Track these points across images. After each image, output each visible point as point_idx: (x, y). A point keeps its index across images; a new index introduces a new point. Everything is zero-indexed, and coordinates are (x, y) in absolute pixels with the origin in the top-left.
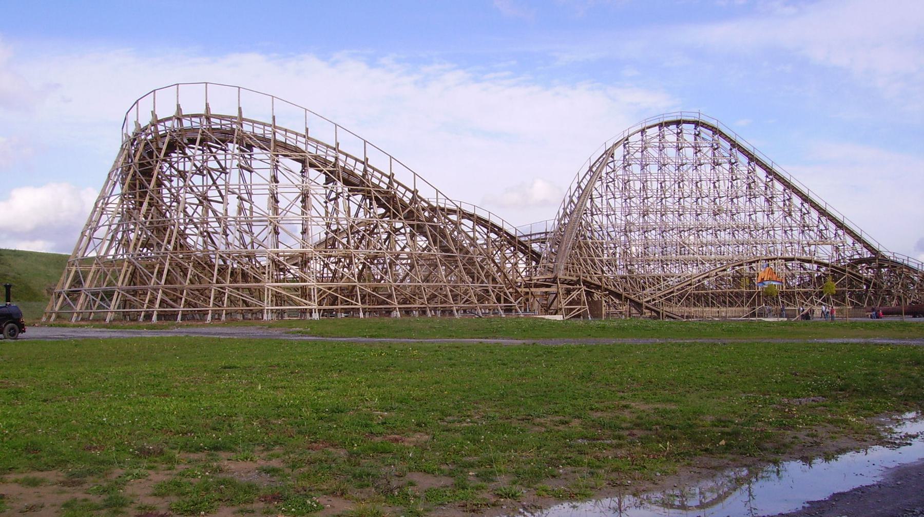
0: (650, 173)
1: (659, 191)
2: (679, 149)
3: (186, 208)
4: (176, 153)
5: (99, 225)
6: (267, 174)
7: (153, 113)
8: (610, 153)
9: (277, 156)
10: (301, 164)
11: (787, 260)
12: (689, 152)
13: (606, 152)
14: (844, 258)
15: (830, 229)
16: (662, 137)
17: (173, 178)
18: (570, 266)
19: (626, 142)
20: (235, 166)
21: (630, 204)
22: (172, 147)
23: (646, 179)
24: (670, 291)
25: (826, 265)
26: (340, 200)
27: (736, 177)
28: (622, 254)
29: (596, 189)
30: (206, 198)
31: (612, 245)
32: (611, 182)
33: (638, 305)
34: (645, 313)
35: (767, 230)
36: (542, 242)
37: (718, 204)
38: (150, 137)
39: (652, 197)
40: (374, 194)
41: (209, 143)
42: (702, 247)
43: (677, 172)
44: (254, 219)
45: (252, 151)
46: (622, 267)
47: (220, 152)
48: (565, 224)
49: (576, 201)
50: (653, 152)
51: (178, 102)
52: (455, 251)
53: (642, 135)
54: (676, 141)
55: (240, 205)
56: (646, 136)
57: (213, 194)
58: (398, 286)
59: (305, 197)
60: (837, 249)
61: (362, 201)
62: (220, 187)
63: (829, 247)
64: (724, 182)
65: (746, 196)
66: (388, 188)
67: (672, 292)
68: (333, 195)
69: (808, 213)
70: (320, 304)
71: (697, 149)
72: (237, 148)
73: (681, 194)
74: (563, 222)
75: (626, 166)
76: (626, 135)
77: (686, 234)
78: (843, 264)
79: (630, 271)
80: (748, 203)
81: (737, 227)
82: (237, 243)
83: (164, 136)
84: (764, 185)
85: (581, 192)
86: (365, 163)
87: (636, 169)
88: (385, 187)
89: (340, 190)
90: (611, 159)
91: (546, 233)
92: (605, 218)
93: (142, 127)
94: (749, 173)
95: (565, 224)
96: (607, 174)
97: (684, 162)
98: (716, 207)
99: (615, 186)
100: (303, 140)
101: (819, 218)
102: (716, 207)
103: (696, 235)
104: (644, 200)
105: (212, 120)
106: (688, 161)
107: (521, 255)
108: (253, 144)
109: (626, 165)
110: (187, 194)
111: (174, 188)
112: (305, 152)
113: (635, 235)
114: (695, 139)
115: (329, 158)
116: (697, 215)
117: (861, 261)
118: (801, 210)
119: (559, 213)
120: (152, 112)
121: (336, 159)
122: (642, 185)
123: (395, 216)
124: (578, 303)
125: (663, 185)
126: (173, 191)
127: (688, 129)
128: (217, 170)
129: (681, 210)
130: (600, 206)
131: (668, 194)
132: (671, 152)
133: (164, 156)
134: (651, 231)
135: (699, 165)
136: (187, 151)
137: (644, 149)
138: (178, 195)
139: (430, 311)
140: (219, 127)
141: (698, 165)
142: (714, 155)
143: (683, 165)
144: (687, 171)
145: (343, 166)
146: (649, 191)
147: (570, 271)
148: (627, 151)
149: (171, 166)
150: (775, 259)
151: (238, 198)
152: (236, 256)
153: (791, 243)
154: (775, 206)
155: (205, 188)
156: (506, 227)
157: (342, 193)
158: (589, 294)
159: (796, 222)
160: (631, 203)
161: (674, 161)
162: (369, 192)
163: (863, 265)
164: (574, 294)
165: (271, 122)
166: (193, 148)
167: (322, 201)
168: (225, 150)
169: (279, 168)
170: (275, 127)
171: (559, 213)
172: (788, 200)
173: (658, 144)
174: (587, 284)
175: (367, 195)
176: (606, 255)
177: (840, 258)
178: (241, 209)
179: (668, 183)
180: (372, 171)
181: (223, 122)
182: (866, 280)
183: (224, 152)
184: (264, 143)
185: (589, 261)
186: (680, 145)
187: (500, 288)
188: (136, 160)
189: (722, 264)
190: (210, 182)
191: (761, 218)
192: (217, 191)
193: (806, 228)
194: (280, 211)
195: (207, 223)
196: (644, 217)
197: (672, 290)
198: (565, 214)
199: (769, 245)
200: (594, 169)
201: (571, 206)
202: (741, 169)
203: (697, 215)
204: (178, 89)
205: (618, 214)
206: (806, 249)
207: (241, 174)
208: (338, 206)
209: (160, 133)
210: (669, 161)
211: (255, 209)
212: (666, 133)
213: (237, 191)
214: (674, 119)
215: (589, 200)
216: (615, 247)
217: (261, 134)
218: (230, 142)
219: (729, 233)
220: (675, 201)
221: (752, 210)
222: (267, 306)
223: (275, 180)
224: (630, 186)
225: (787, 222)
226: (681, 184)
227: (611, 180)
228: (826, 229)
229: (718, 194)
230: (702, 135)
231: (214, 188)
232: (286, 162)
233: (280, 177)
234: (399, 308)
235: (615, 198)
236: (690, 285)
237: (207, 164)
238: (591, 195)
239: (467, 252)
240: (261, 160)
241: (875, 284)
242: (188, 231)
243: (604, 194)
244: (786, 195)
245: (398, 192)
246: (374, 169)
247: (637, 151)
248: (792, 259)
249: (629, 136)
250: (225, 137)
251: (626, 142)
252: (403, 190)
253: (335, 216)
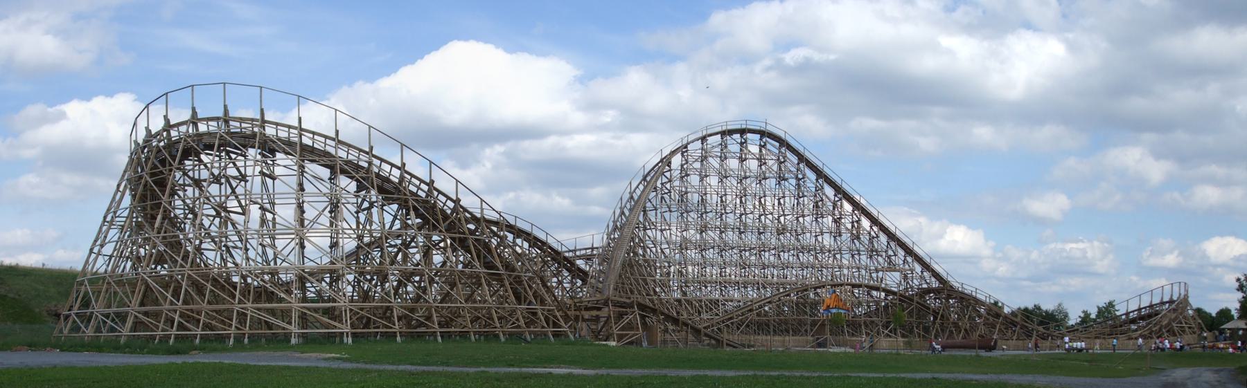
0: (709, 185)
1: (719, 205)
2: (742, 160)
3: (202, 220)
4: (191, 160)
5: (107, 241)
6: (293, 181)
7: (166, 117)
8: (666, 161)
9: (303, 161)
10: (329, 170)
11: (854, 286)
12: (753, 164)
13: (662, 161)
14: (912, 287)
15: (899, 255)
16: (724, 146)
17: (186, 188)
18: (620, 285)
19: (684, 150)
20: (257, 173)
21: (687, 219)
22: (187, 154)
23: (706, 191)
24: (729, 316)
25: (894, 293)
26: (374, 210)
27: (803, 193)
28: (677, 273)
29: (650, 201)
30: (225, 210)
31: (666, 264)
32: (667, 193)
33: (697, 331)
34: (704, 341)
35: (836, 252)
36: (588, 259)
37: (783, 222)
38: (162, 144)
39: (711, 212)
40: (412, 203)
41: (228, 148)
42: (764, 269)
43: (739, 185)
44: (277, 232)
45: (274, 156)
46: (676, 288)
47: (240, 158)
48: (614, 238)
49: (627, 213)
50: (714, 162)
51: (193, 104)
52: (501, 268)
53: (702, 144)
54: (739, 151)
55: (263, 216)
56: (707, 144)
57: (232, 204)
58: (438, 307)
59: (335, 207)
60: (905, 277)
61: (398, 210)
62: (240, 197)
63: (897, 274)
64: (790, 199)
65: (813, 215)
66: (427, 196)
67: (731, 318)
68: (366, 205)
69: (877, 237)
70: (352, 326)
71: (761, 161)
72: (259, 154)
73: (742, 209)
74: (612, 236)
75: (684, 177)
76: (685, 142)
77: (747, 254)
78: (911, 293)
79: (685, 294)
80: (814, 223)
81: (803, 248)
82: (259, 259)
83: (178, 142)
84: (832, 204)
85: (633, 203)
86: (402, 168)
87: (694, 179)
88: (423, 195)
89: (374, 199)
90: (667, 167)
91: (593, 249)
92: (659, 233)
93: (153, 133)
94: (816, 190)
95: (614, 238)
96: (662, 184)
97: (748, 174)
98: (780, 226)
99: (670, 198)
100: (333, 143)
101: (888, 243)
102: (780, 226)
103: (758, 256)
104: (702, 214)
105: (231, 123)
106: (752, 174)
107: (566, 273)
108: (277, 148)
109: (684, 174)
110: (205, 205)
111: (190, 199)
112: (334, 157)
113: (692, 254)
114: (761, 151)
115: (361, 163)
116: (760, 233)
117: (929, 291)
118: (870, 233)
119: (608, 226)
120: (164, 116)
121: (370, 164)
122: (700, 198)
123: (435, 228)
124: (631, 329)
125: (724, 199)
126: (188, 201)
127: (753, 140)
128: (235, 178)
129: (742, 227)
130: (653, 220)
131: (728, 210)
132: (733, 163)
133: (179, 165)
134: (709, 249)
135: (763, 179)
136: (203, 157)
137: (704, 158)
138: (194, 206)
139: (474, 335)
140: (239, 130)
141: (762, 178)
142: (780, 169)
143: (746, 178)
144: (750, 184)
145: (377, 171)
146: (708, 205)
147: (620, 292)
148: (686, 160)
149: (185, 174)
150: (841, 285)
151: (260, 208)
152: (259, 273)
153: (858, 268)
154: (842, 227)
155: (223, 199)
156: (551, 241)
157: (376, 202)
158: (643, 317)
159: (864, 246)
160: (689, 217)
161: (737, 173)
162: (406, 201)
163: (931, 295)
164: (626, 320)
165: (296, 124)
166: (211, 155)
167: (353, 209)
168: (245, 156)
169: (305, 174)
170: (302, 130)
171: (608, 226)
172: (857, 222)
173: (719, 154)
174: (642, 307)
175: (404, 205)
176: (659, 274)
177: (908, 286)
178: (263, 221)
179: (729, 198)
180: (409, 177)
181: (243, 125)
182: (934, 311)
183: (243, 158)
184: (288, 147)
185: (640, 281)
186: (743, 156)
187: (549, 310)
188: (147, 170)
189: (784, 288)
190: (229, 191)
191: (827, 240)
192: (236, 201)
193: (874, 253)
194: (306, 222)
195: (226, 237)
196: (701, 233)
197: (732, 315)
198: (615, 229)
199: (836, 270)
200: (648, 179)
201: (622, 219)
202: (808, 185)
203: (760, 233)
204: (193, 90)
205: (674, 229)
206: (874, 275)
207: (264, 183)
208: (371, 216)
209: (173, 139)
210: (732, 173)
211: (278, 220)
212: (729, 142)
213: (260, 201)
214: (738, 127)
215: (642, 213)
216: (670, 267)
217: (286, 138)
218: (251, 147)
219: (794, 255)
220: (736, 217)
221: (818, 230)
222: (294, 329)
223: (301, 188)
224: (687, 199)
225: (855, 245)
226: (743, 199)
227: (667, 191)
228: (895, 255)
229: (783, 211)
230: (768, 146)
231: (234, 198)
232: (313, 168)
233: (307, 185)
234: (440, 332)
235: (671, 211)
236: (751, 310)
237: (226, 172)
238: (645, 207)
239: (513, 270)
240: (285, 166)
241: (942, 316)
242: (203, 246)
243: (658, 206)
244: (854, 216)
245: (438, 201)
246: (412, 176)
247: (696, 160)
248: (859, 286)
249: (688, 143)
250: (245, 141)
251: (684, 150)
252: (443, 199)
253: (368, 227)
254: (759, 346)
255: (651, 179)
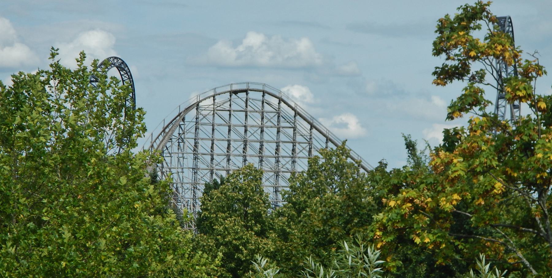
8: (181, 116)
200: (167, 130)
254: (34, 259)
255: (169, 131)
